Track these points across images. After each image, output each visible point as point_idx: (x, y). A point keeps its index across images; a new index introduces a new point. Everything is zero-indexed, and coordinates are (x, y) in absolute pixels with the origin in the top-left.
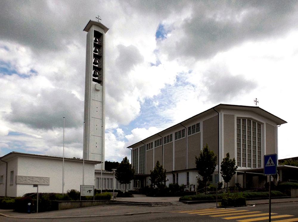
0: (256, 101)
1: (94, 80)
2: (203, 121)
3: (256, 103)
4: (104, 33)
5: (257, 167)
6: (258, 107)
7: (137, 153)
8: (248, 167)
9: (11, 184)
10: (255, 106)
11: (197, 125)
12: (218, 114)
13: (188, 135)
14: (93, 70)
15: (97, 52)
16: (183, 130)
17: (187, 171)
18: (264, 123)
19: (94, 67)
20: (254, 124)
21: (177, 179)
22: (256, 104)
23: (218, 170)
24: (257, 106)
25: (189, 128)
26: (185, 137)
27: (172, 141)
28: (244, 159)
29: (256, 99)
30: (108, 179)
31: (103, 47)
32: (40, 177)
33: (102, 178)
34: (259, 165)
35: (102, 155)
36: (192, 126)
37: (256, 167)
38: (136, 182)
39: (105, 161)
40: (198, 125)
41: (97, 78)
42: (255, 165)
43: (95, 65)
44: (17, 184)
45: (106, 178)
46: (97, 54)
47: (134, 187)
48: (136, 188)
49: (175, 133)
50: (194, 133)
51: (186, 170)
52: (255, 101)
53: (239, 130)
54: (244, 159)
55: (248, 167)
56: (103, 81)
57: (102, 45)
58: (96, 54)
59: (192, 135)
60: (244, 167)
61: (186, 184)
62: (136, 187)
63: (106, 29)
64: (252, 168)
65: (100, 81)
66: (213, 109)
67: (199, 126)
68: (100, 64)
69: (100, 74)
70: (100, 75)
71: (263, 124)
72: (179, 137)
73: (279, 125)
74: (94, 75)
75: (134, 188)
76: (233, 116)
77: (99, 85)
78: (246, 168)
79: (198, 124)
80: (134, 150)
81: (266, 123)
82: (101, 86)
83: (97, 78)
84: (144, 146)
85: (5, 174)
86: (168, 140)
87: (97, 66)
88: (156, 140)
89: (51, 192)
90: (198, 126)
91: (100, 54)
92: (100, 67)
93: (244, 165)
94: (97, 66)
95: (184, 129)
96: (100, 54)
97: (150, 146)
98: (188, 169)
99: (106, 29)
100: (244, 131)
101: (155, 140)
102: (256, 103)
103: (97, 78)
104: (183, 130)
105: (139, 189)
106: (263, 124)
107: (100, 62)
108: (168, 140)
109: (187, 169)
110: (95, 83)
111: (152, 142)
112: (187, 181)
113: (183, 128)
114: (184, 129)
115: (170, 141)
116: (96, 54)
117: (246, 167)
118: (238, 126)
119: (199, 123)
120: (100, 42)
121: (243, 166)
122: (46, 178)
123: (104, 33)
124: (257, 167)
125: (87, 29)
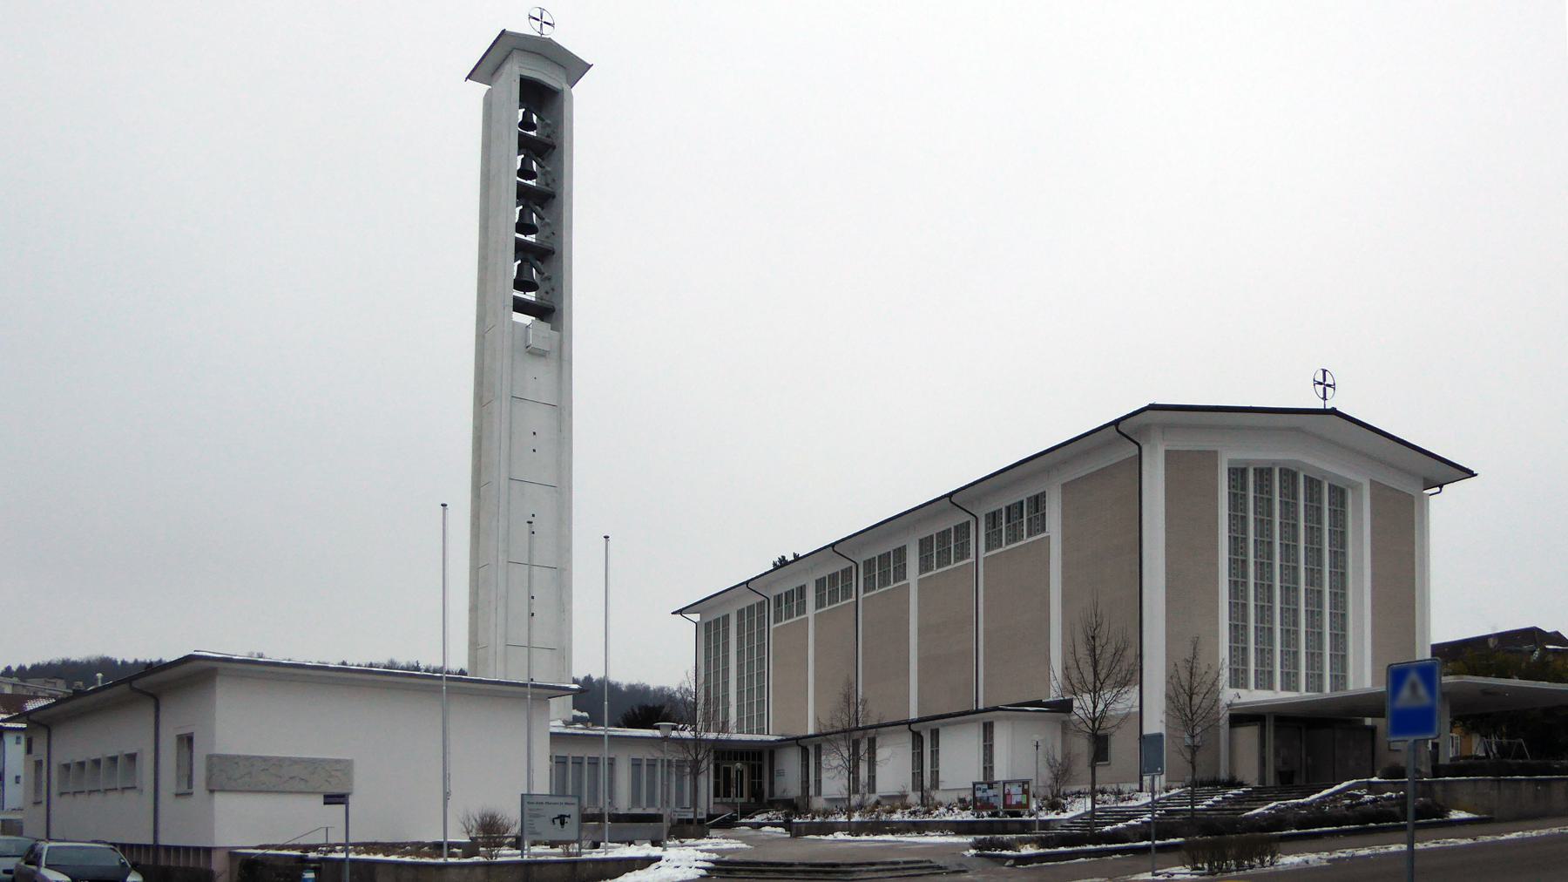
0: (1324, 384)
1: (520, 307)
2: (1064, 486)
3: (1325, 389)
4: (566, 87)
5: (1327, 689)
6: (1334, 411)
7: (726, 636)
8: (1282, 689)
9: (180, 792)
10: (1319, 405)
11: (799, 593)
12: (1137, 452)
13: (865, 592)
14: (516, 261)
15: (531, 175)
16: (963, 530)
17: (985, 719)
18: (1361, 484)
19: (521, 247)
20: (1316, 489)
21: (935, 754)
22: (1325, 398)
23: (1138, 709)
24: (1329, 407)
25: (993, 518)
26: (972, 559)
27: (805, 613)
28: (1264, 654)
29: (1324, 371)
30: (578, 762)
31: (561, 152)
32: (313, 762)
33: (663, 760)
34: (1334, 678)
35: (562, 652)
36: (786, 593)
37: (1320, 689)
38: (727, 771)
39: (1219, 449)
40: (1038, 502)
41: (531, 296)
42: (1315, 681)
43: (522, 237)
44: (212, 791)
45: (582, 758)
46: (532, 183)
47: (717, 795)
48: (725, 800)
49: (921, 541)
50: (789, 618)
51: (977, 711)
52: (1320, 383)
53: (1238, 520)
54: (1264, 654)
55: (1282, 689)
56: (561, 310)
57: (556, 143)
58: (529, 182)
59: (828, 610)
60: (1263, 688)
61: (982, 780)
62: (727, 794)
63: (576, 68)
64: (1302, 694)
65: (547, 312)
66: (1113, 427)
67: (905, 559)
68: (547, 231)
69: (546, 275)
70: (549, 279)
71: (1357, 487)
72: (797, 611)
73: (1438, 489)
74: (521, 284)
75: (718, 800)
76: (1212, 456)
77: (544, 327)
78: (1276, 692)
79: (1037, 497)
80: (708, 625)
81: (1372, 482)
82: (555, 333)
83: (533, 294)
84: (761, 604)
85: (46, 756)
86: (789, 609)
87: (531, 238)
88: (825, 572)
89: (467, 612)
90: (779, 606)
91: (547, 185)
92: (547, 245)
93: (1265, 681)
94: (531, 238)
95: (968, 523)
96: (547, 185)
97: (792, 601)
98: (986, 710)
99: (576, 68)
100: (1264, 526)
101: (925, 534)
102: (1325, 389)
103: (531, 296)
104: (963, 530)
105: (742, 804)
106: (1357, 487)
107: (547, 220)
108: (789, 609)
109: (981, 707)
110: (526, 319)
111: (726, 613)
112: (985, 761)
113: (962, 518)
114: (968, 523)
115: (952, 562)
116: (529, 182)
117: (1271, 687)
118: (1237, 501)
119: (1044, 494)
120: (548, 130)
121: (1256, 688)
122: (338, 761)
123: (566, 87)
124: (1327, 689)
125: (484, 70)
